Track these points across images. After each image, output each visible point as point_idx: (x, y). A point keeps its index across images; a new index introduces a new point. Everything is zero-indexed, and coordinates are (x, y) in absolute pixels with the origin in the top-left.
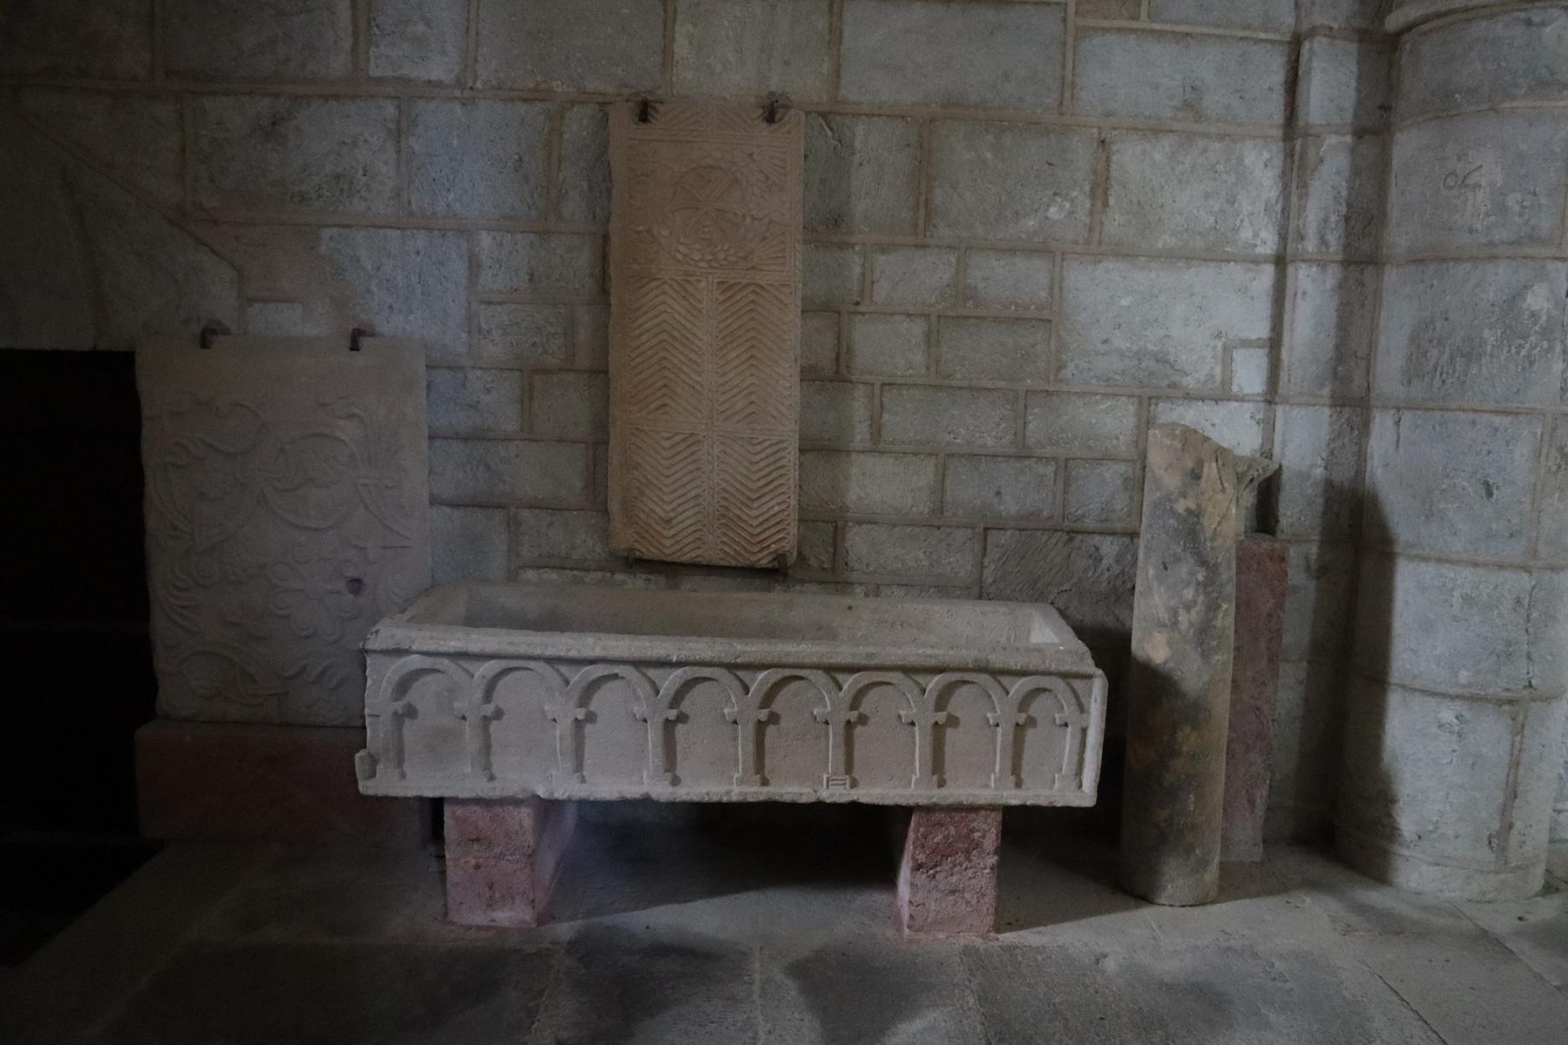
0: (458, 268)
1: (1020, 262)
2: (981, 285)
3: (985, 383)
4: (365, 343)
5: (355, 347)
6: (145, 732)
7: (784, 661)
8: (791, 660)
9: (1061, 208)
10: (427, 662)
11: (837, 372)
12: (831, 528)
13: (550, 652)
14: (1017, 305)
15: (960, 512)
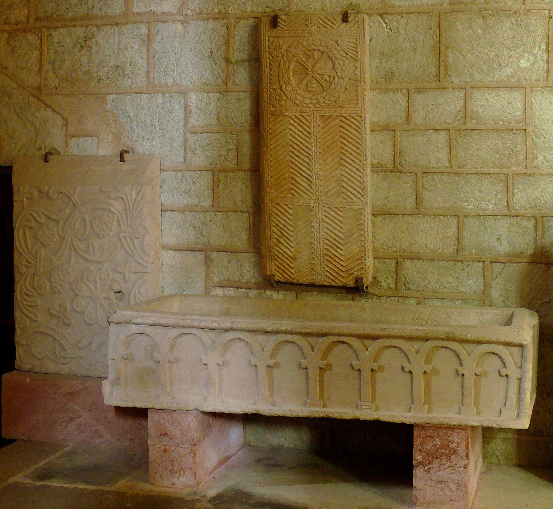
0: (180, 114)
1: (505, 95)
2: (480, 110)
3: (485, 170)
4: (126, 157)
5: (122, 159)
6: (6, 376)
7: (332, 331)
8: (336, 331)
9: (528, 60)
10: (139, 329)
11: (395, 166)
12: (393, 263)
13: (203, 324)
14: (502, 120)
15: (474, 252)
